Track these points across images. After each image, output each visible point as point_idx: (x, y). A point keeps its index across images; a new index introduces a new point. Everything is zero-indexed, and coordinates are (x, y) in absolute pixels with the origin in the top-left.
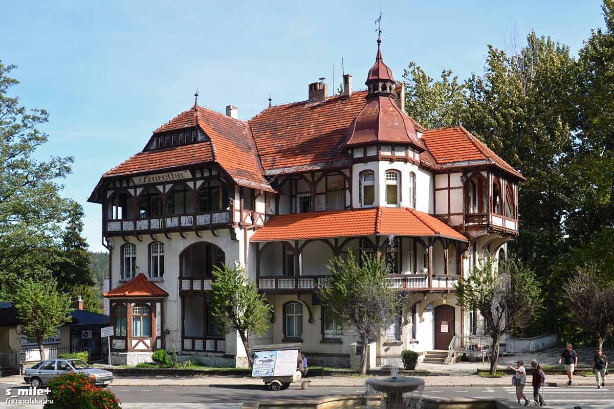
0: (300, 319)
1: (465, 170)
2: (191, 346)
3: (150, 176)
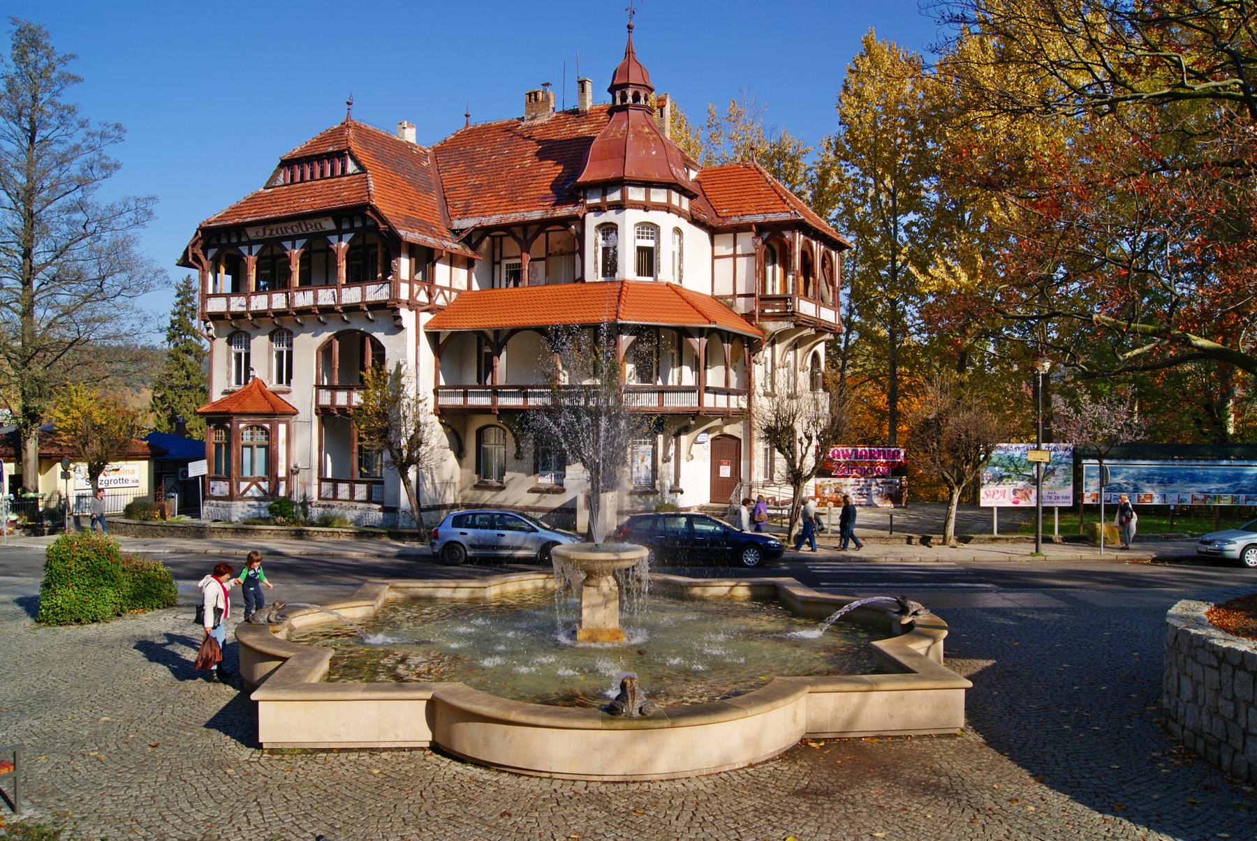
1: (761, 228)
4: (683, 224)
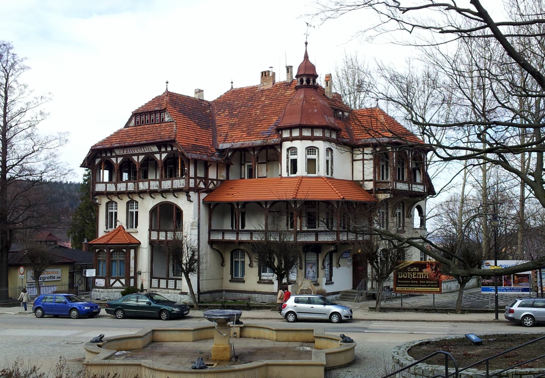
0: (243, 262)
1: (375, 146)
2: (157, 284)
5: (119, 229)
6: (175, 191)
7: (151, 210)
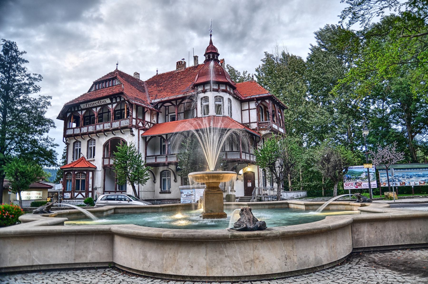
0: (170, 180)
1: (257, 99)
3: (89, 103)
4: (231, 98)
5: (82, 159)
6: (121, 129)
7: (104, 144)
